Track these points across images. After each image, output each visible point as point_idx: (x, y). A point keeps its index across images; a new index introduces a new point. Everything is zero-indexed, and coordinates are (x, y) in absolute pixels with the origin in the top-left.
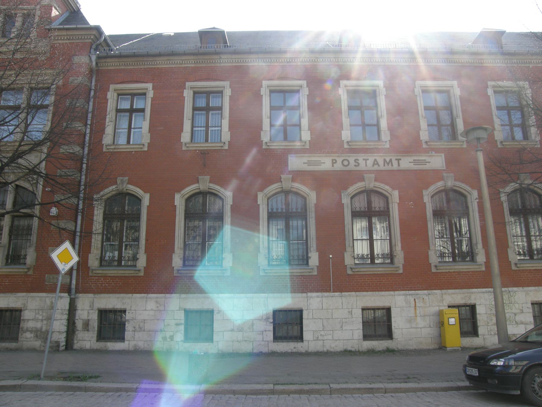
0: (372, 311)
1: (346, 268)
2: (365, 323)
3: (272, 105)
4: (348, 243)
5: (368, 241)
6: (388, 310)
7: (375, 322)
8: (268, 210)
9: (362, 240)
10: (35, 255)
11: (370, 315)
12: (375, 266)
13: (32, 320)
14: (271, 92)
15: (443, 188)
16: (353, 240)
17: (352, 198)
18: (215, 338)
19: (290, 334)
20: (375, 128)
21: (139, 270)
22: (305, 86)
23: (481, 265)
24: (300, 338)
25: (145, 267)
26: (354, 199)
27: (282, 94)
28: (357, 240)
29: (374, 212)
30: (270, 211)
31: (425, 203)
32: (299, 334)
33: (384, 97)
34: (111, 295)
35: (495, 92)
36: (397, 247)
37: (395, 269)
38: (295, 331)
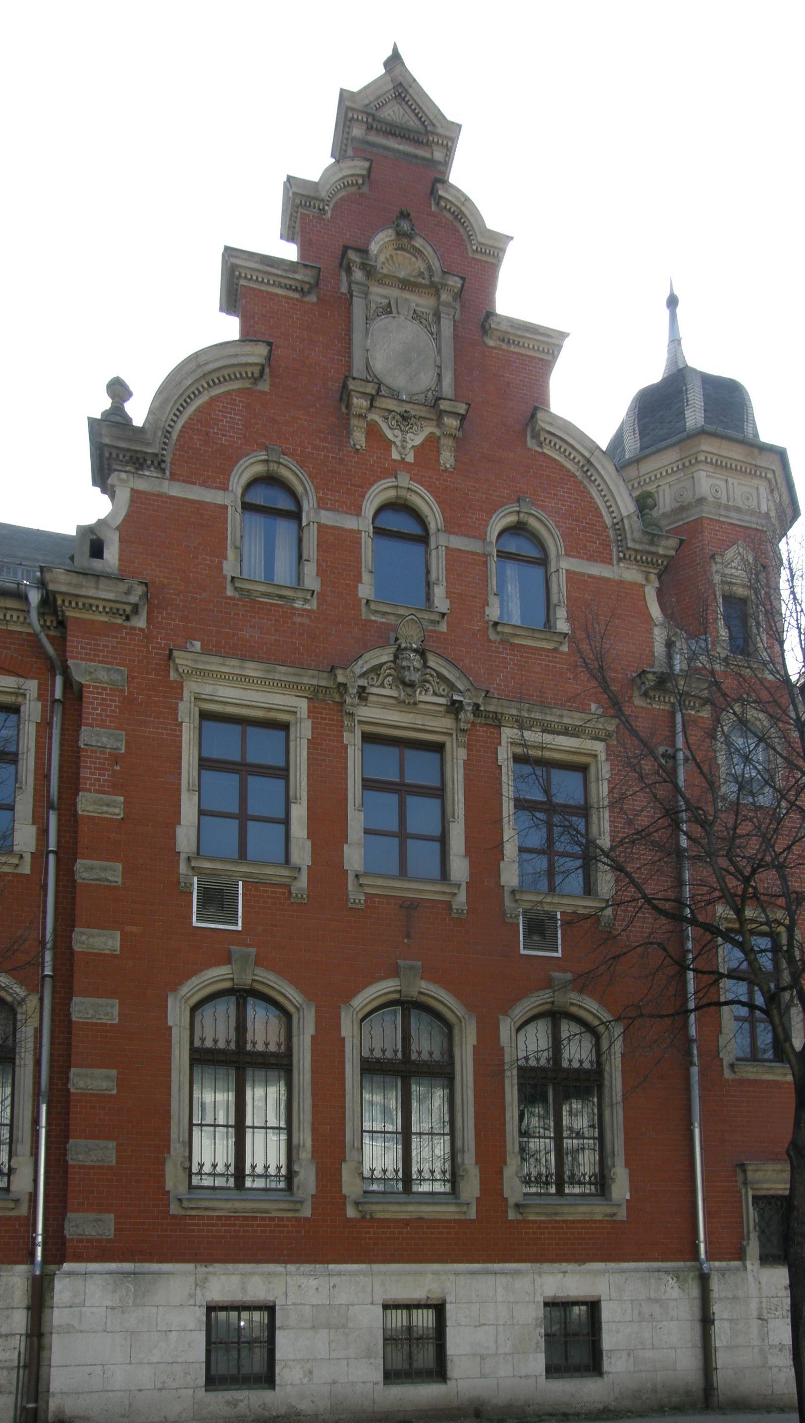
0: (404, 1311)
1: (344, 1204)
2: (214, 1343)
3: (205, 754)
4: (177, 1130)
5: (400, 1136)
6: (594, 1306)
7: (409, 1339)
8: (192, 1042)
9: (385, 1132)
10: (627, 1170)
11: (399, 1319)
12: (411, 1198)
13: (565, 1318)
14: (205, 716)
15: (396, 996)
16: (191, 1125)
17: (194, 1010)
18: (606, 1366)
19: (245, 1370)
20: (437, 845)
21: (17, 1201)
22: (602, 757)
23: (619, 1205)
24: (268, 1379)
25: (477, 1199)
26: (198, 1013)
27: (238, 728)
28: (201, 1125)
29: (251, 1054)
30: (366, 1054)
31: (170, 1028)
32: (264, 1370)
33: (305, 742)
34: (546, 1266)
35: (518, 759)
36: (466, 1155)
37: (291, 1206)
38: (256, 1363)
